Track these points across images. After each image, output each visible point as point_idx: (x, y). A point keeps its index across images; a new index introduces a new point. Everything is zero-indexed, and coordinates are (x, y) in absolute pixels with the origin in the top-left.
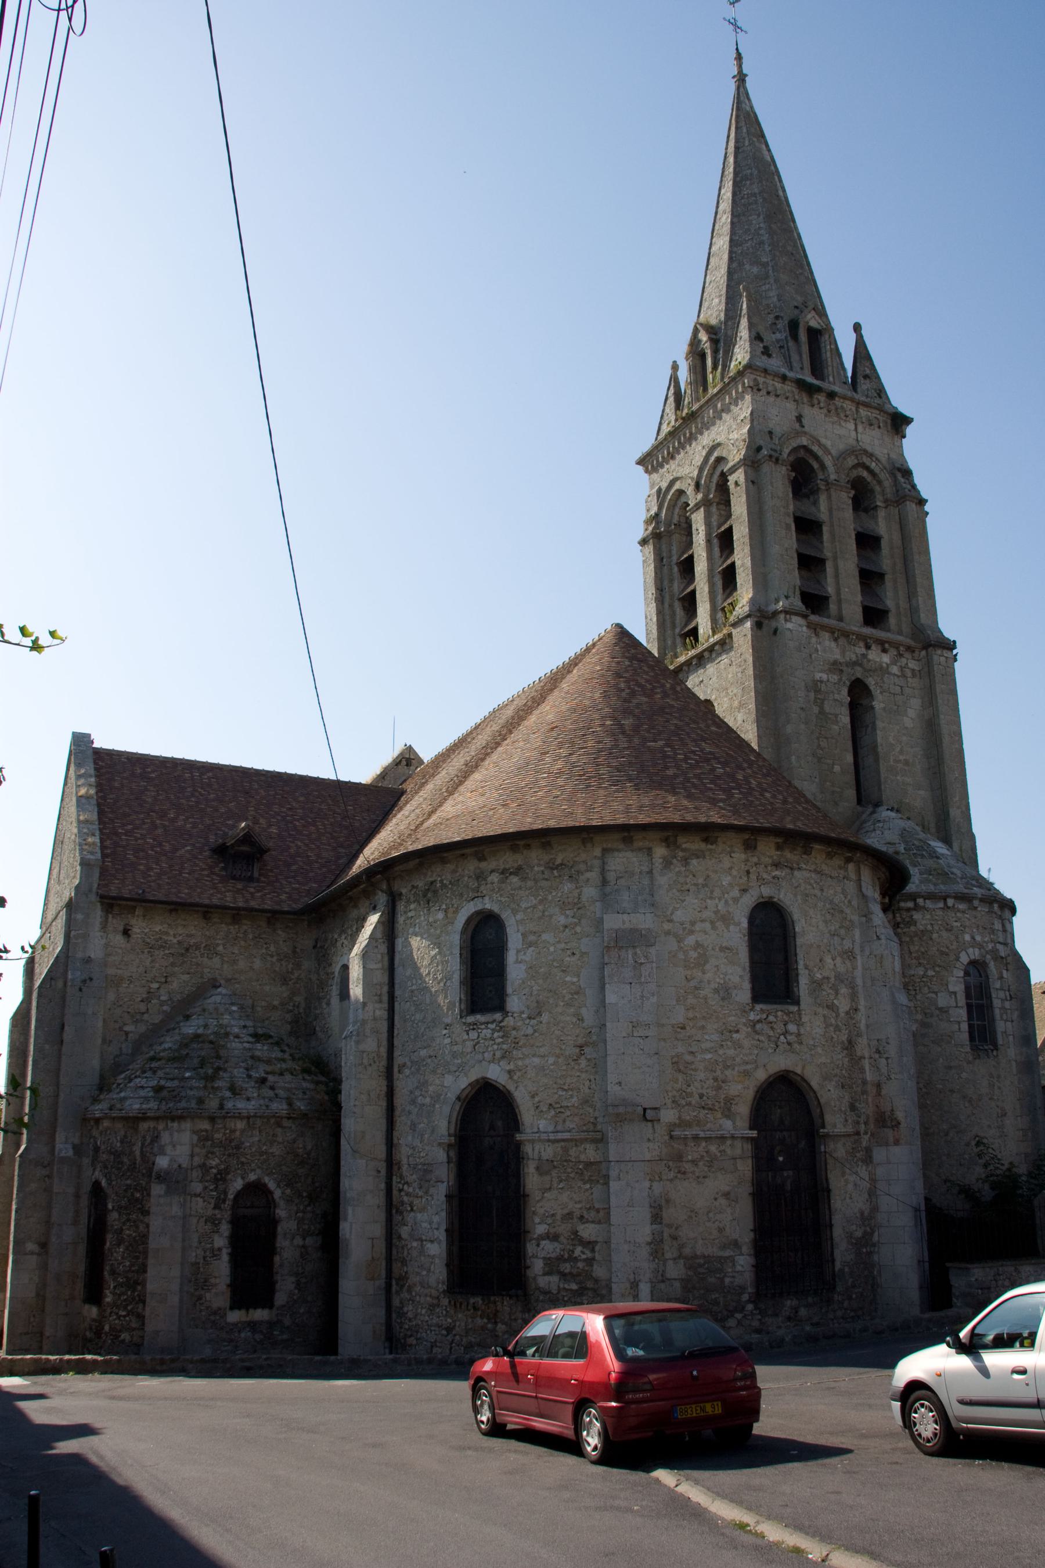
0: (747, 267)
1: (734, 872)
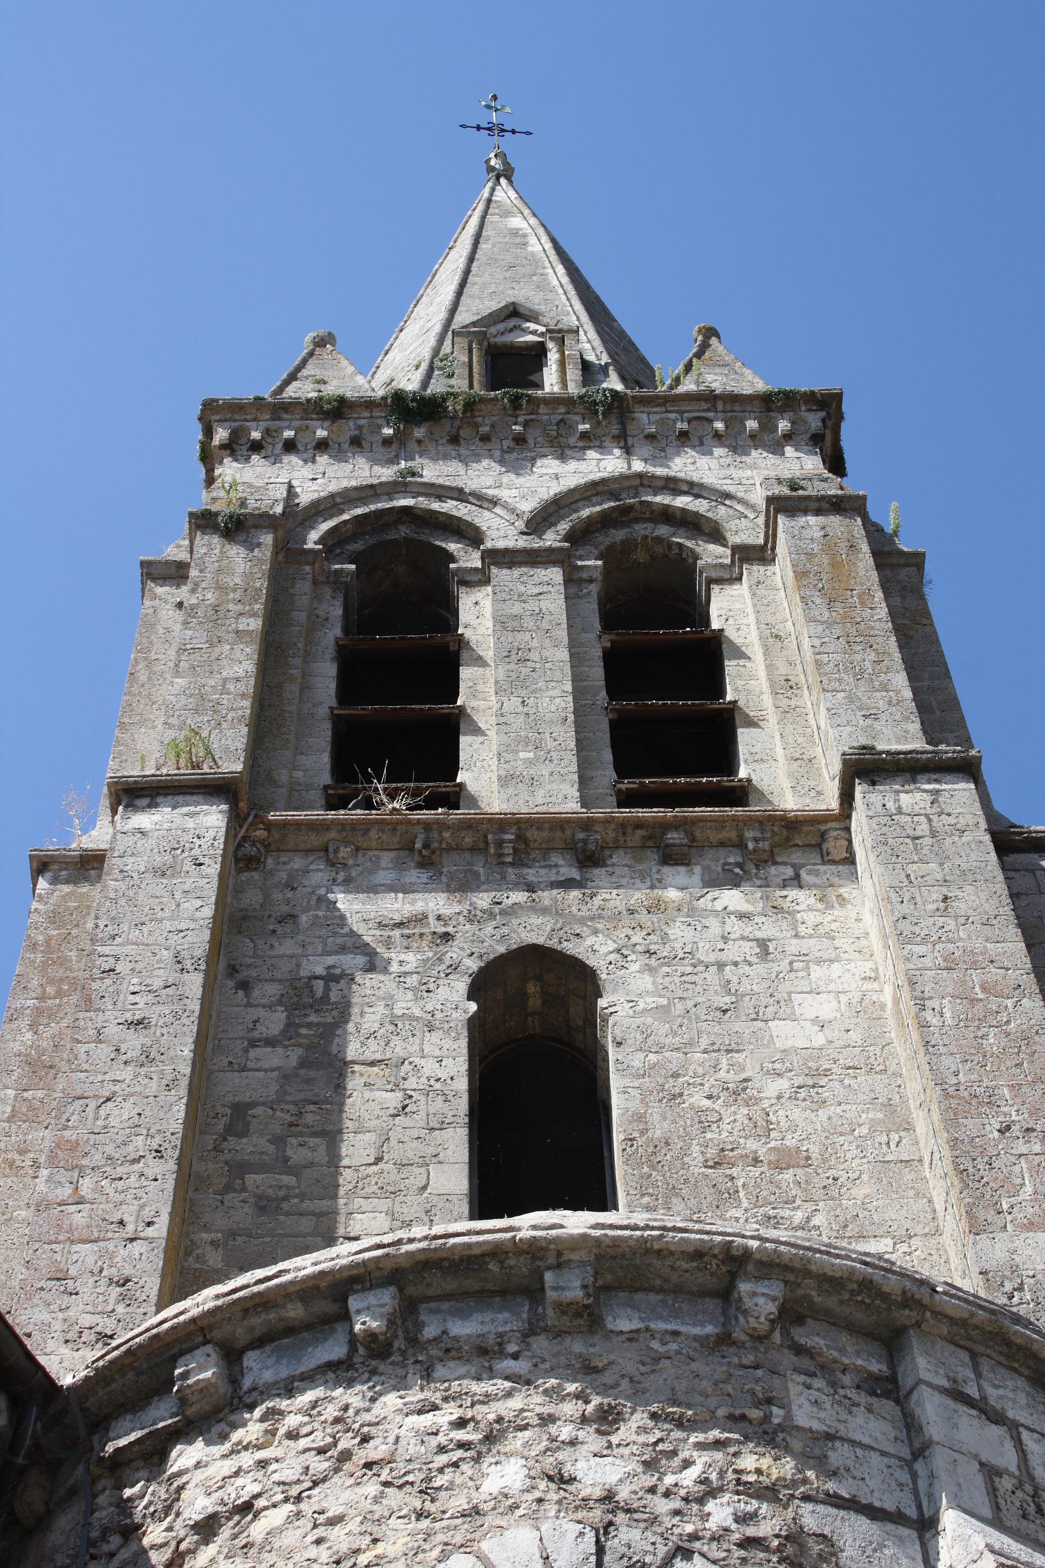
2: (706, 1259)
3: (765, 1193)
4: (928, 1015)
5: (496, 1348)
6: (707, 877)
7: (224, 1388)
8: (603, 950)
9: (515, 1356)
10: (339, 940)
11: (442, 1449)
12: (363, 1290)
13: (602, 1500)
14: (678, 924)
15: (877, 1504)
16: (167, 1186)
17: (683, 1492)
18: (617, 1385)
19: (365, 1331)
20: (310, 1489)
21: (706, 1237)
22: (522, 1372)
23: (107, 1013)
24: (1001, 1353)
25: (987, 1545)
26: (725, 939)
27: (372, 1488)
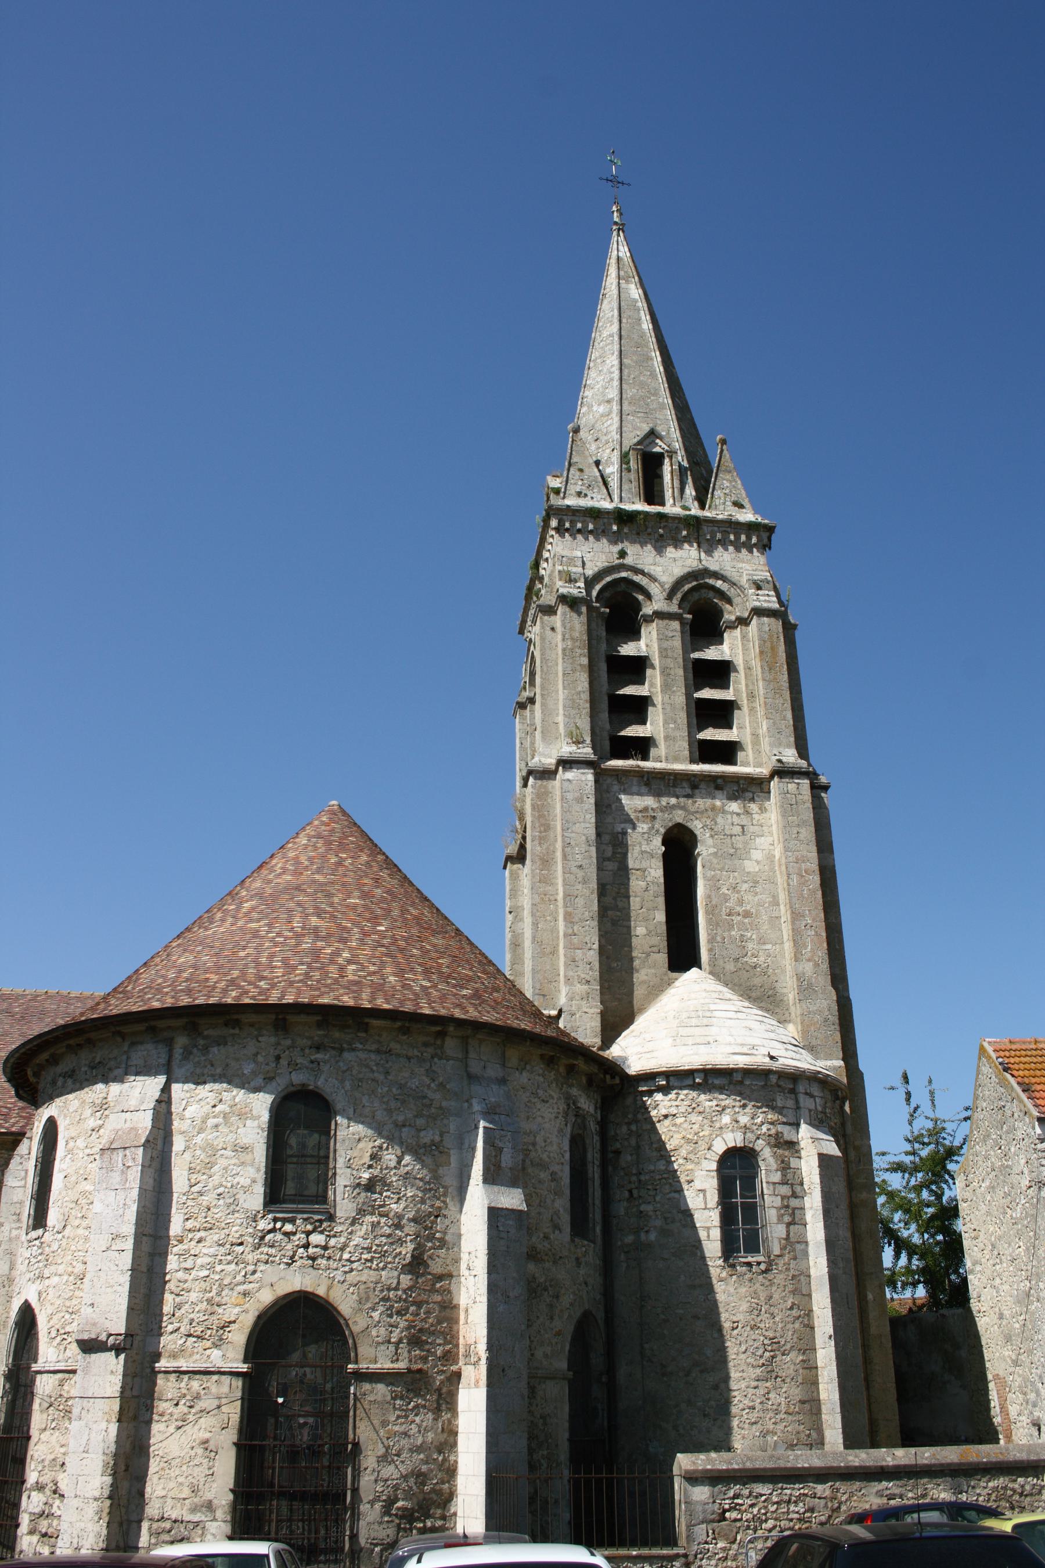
0: (595, 408)
1: (260, 1058)
27: (701, 1118)
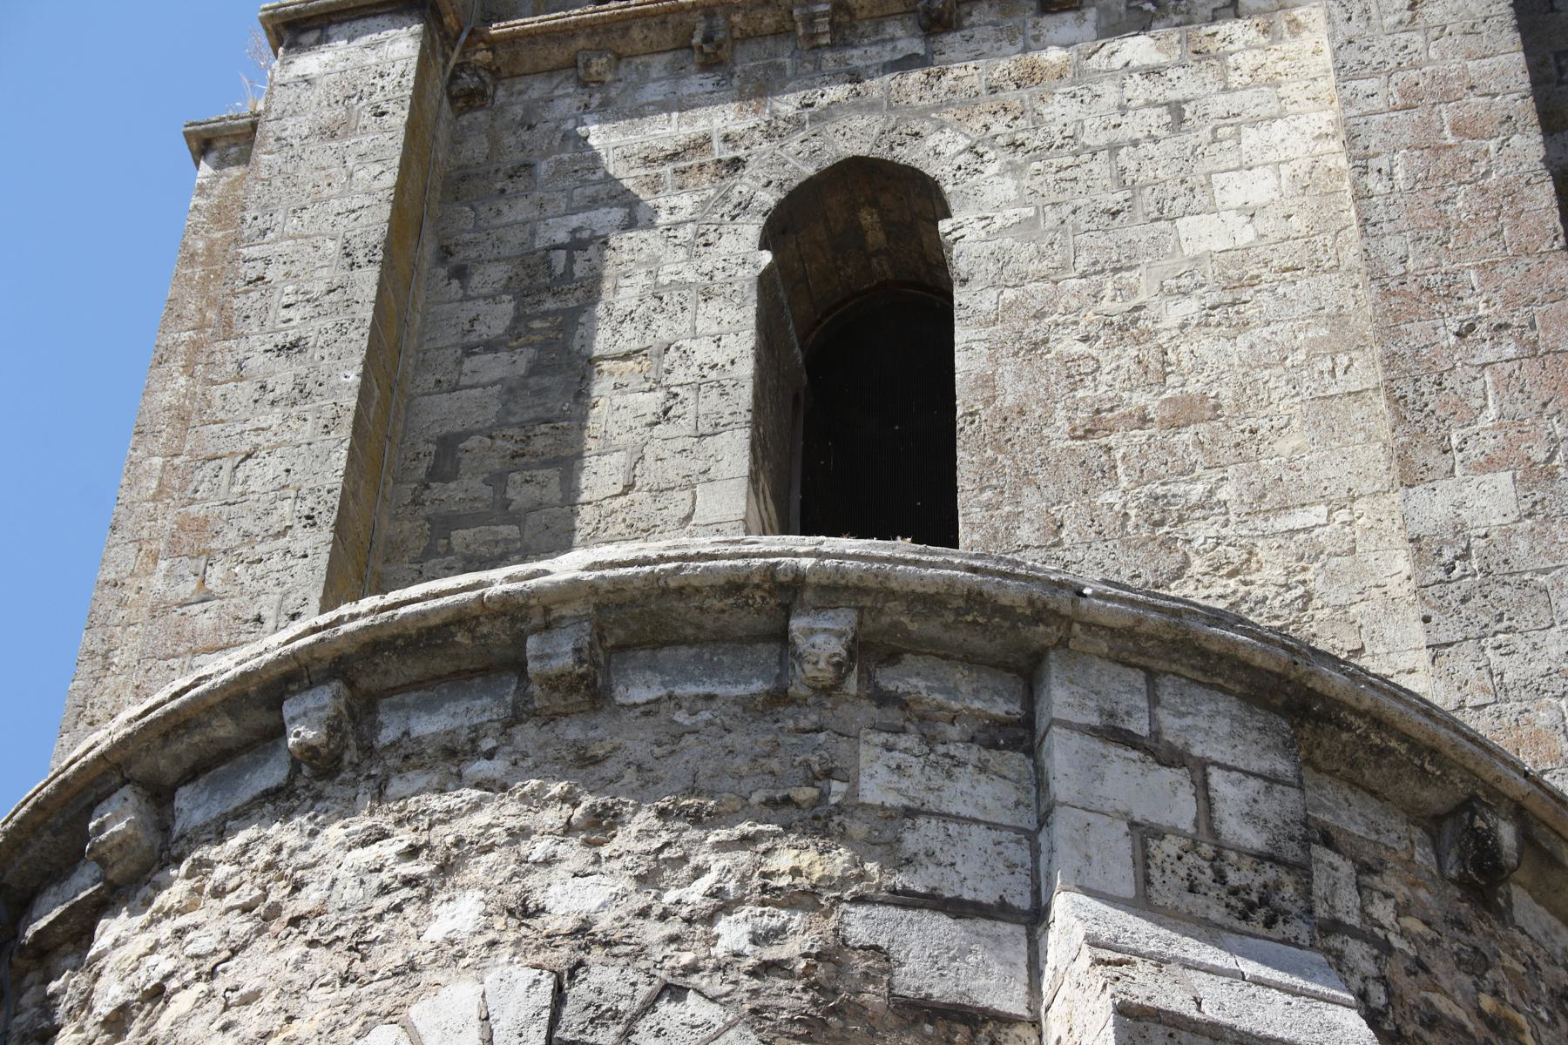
2: (746, 592)
3: (1152, 464)
4: (1372, 181)
5: (467, 747)
6: (1103, 23)
7: (148, 839)
8: (951, 150)
9: (490, 755)
10: (590, 191)
11: (384, 890)
12: (299, 692)
13: (573, 934)
14: (1058, 97)
15: (968, 895)
16: (319, 562)
17: (685, 911)
18: (620, 777)
19: (300, 744)
20: (227, 960)
21: (740, 563)
22: (496, 775)
23: (251, 339)
24: (1193, 667)
25: (1087, 937)
26: (1123, 109)
